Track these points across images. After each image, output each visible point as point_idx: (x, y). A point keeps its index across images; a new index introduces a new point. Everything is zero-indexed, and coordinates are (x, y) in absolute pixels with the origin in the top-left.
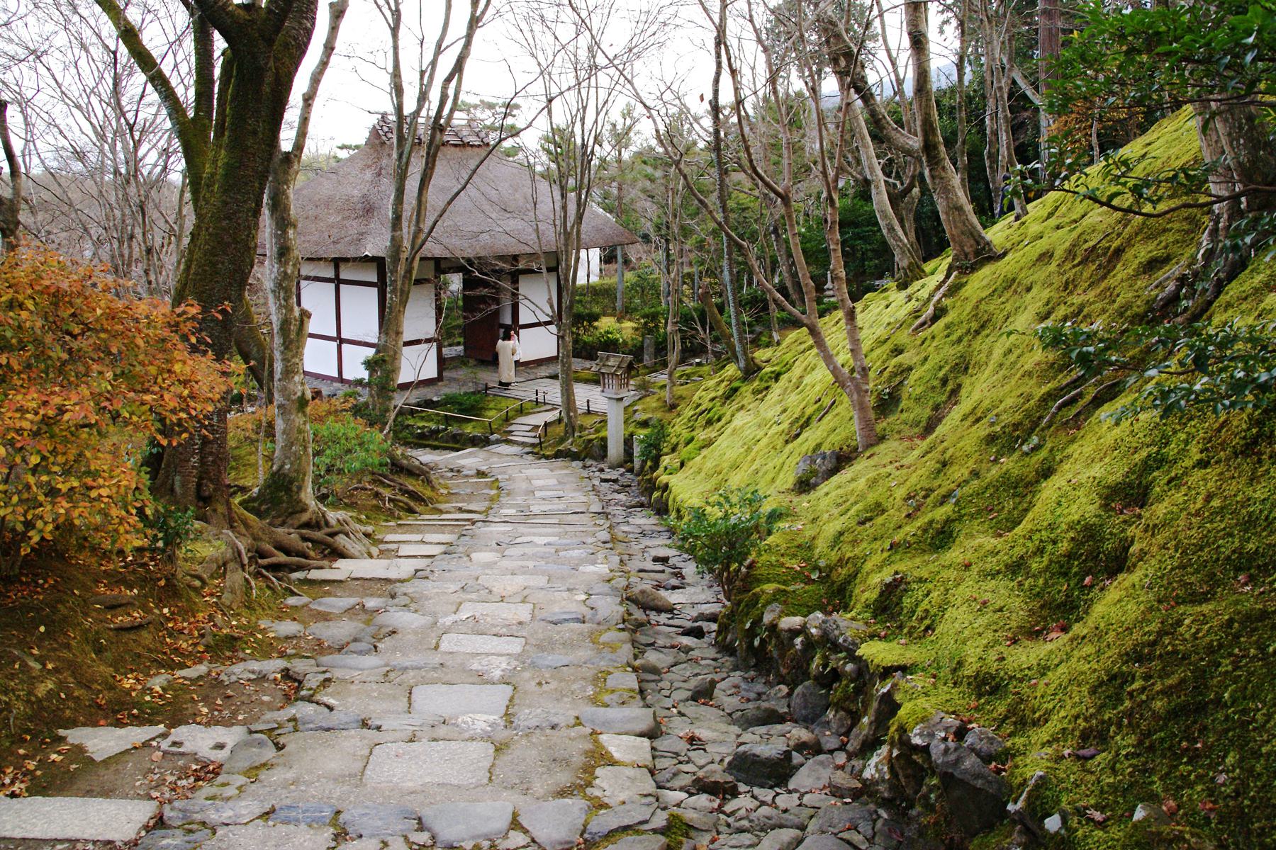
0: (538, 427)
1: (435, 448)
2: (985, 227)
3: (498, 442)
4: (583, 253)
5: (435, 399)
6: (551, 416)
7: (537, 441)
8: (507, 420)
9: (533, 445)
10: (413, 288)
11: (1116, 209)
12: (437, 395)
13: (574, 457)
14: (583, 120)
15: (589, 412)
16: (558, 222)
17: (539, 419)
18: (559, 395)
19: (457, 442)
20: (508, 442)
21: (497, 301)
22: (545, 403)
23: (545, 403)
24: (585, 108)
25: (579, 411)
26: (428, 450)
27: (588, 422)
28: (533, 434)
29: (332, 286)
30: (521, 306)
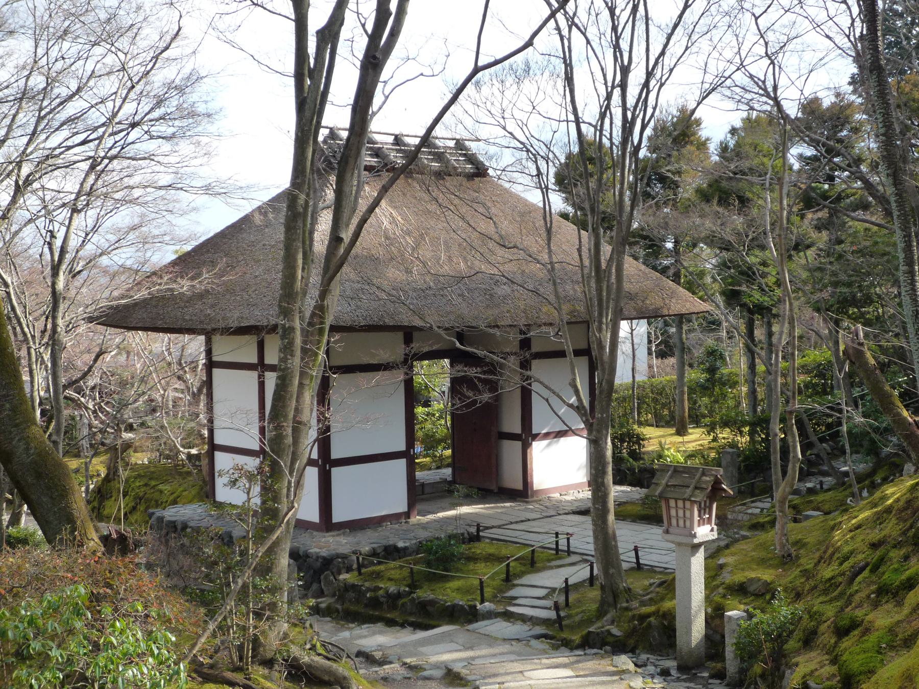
0: (553, 590)
1: (391, 623)
2: (253, 662)
3: (490, 615)
4: (624, 325)
5: (401, 544)
6: (580, 573)
7: (552, 615)
8: (509, 579)
9: (545, 622)
10: (590, 505)
11: (491, 559)
12: (404, 539)
13: (619, 647)
14: (623, 86)
15: (639, 566)
16: (587, 262)
17: (553, 578)
18: (591, 540)
19: (428, 615)
20: (508, 616)
21: (493, 386)
22: (569, 552)
23: (569, 552)
24: (625, 71)
25: (625, 566)
26: (380, 626)
27: (638, 584)
28: (548, 603)
29: (254, 375)
30: (534, 397)
